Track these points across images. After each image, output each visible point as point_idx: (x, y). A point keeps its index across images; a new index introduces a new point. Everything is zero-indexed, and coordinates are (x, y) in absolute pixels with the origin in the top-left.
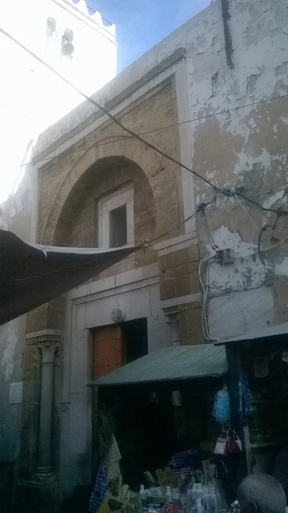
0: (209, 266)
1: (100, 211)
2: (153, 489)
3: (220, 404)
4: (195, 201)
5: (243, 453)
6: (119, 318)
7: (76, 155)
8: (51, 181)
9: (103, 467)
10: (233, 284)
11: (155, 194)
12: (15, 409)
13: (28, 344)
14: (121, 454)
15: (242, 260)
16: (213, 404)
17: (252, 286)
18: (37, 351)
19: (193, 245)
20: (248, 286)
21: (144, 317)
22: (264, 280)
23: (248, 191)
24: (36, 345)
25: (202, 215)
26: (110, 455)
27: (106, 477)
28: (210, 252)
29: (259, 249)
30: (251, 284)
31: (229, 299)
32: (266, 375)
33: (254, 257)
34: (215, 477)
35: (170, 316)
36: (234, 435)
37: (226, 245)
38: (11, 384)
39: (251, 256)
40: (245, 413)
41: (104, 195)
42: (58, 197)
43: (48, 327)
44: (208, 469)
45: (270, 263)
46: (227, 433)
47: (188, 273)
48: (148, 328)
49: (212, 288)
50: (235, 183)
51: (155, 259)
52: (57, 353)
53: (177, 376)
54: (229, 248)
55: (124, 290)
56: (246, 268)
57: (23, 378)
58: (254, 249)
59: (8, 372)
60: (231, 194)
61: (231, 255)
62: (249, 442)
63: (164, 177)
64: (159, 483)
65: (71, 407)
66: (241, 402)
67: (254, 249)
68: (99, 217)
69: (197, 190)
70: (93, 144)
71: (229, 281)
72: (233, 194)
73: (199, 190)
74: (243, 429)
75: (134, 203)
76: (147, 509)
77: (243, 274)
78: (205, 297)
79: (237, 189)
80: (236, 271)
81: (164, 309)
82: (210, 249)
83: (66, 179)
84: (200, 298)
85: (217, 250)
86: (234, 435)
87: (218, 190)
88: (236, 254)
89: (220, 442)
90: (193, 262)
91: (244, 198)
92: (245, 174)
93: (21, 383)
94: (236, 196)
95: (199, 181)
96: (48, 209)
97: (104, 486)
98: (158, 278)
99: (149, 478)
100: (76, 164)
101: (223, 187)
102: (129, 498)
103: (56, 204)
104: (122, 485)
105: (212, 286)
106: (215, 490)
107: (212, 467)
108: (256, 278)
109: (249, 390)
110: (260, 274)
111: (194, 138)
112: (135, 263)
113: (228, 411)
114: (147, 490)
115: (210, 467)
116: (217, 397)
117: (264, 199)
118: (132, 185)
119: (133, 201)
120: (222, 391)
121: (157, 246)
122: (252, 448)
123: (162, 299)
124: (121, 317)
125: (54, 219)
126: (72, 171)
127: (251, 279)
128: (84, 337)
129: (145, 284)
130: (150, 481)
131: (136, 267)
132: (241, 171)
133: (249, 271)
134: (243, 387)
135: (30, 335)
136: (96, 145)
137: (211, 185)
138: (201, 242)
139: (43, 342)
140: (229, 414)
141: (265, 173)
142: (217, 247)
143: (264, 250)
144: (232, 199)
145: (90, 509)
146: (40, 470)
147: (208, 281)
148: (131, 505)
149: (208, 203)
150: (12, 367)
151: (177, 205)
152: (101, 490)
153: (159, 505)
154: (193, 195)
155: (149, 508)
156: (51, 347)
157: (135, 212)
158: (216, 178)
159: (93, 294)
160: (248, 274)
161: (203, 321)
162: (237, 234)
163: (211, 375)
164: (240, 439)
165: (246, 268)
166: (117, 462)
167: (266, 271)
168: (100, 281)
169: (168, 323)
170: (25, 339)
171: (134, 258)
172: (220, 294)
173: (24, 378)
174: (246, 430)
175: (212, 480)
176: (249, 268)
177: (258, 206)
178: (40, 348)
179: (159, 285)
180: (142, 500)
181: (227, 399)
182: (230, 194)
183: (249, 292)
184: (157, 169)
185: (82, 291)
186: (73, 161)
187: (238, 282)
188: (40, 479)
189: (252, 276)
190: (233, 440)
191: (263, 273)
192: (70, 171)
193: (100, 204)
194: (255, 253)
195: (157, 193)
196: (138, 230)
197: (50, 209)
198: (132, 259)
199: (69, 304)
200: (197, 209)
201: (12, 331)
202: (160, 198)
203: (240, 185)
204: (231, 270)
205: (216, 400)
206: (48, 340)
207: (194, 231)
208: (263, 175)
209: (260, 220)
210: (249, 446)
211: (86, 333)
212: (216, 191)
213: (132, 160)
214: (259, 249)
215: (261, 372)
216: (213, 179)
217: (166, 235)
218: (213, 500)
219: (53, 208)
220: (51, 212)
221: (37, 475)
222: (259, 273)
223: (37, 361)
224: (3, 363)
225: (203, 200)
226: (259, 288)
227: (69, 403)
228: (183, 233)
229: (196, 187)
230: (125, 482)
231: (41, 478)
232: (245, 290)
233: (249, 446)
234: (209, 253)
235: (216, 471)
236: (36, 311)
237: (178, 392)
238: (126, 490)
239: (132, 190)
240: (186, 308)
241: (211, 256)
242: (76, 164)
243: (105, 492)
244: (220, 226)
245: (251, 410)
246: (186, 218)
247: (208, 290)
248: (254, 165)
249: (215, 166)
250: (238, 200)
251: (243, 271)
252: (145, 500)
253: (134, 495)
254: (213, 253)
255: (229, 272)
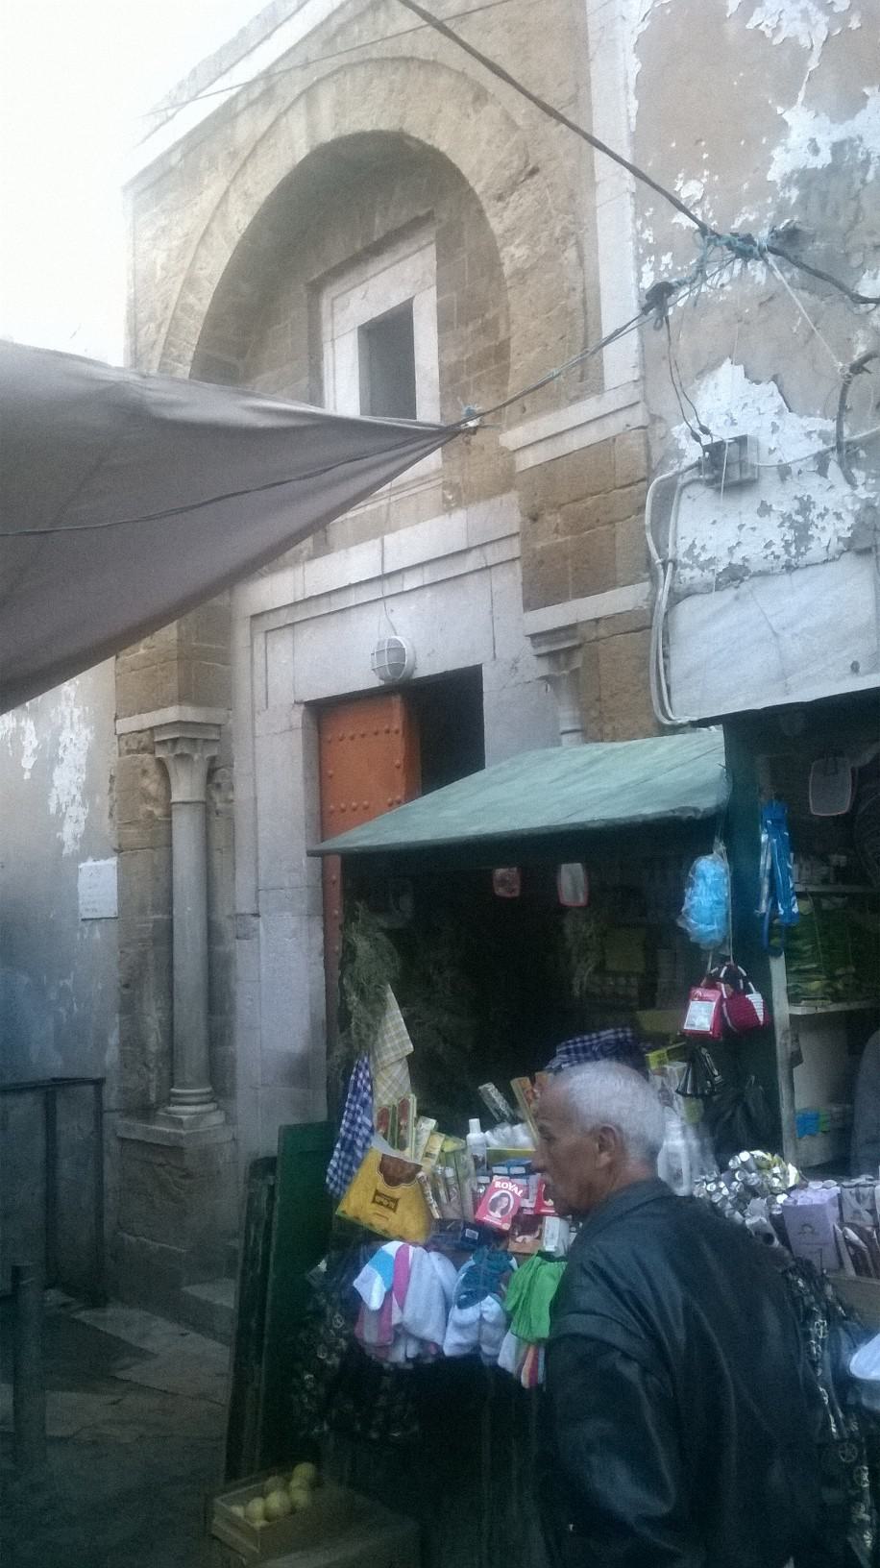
0: (680, 496)
1: (326, 328)
2: (506, 1130)
3: (704, 892)
4: (639, 279)
5: (765, 1032)
6: (397, 667)
7: (245, 130)
8: (163, 229)
9: (361, 1075)
10: (752, 551)
11: (507, 261)
12: (98, 935)
13: (126, 748)
14: (413, 1040)
15: (784, 472)
16: (683, 895)
17: (811, 556)
18: (152, 768)
19: (629, 428)
20: (799, 554)
21: (471, 664)
22: (849, 535)
23: (812, 238)
24: (151, 753)
25: (659, 322)
26: (380, 1040)
27: (370, 1101)
28: (684, 450)
29: (840, 432)
30: (807, 549)
31: (737, 598)
32: (844, 809)
33: (821, 462)
34: (684, 1095)
35: (552, 656)
36: (741, 981)
37: (736, 424)
38: (82, 865)
39: (811, 458)
40: (776, 921)
41: (338, 272)
42: (190, 283)
43: (183, 698)
44: (662, 1072)
45: (872, 478)
46: (722, 975)
47: (611, 523)
48: (485, 697)
49: (685, 566)
50: (770, 214)
51: (506, 480)
52: (215, 775)
53: (577, 819)
54: (744, 434)
55: (411, 582)
56: (796, 498)
57: (117, 847)
58: (823, 436)
59: (70, 833)
60: (756, 250)
61: (751, 457)
62: (786, 1000)
63: (536, 200)
64: (520, 1115)
65: (261, 925)
66: (766, 889)
67: (823, 436)
68: (325, 345)
69: (647, 240)
70: (297, 91)
71: (739, 543)
72: (762, 251)
73: (651, 241)
74: (768, 963)
75: (439, 294)
76: (489, 1181)
77: (786, 518)
78: (663, 595)
79: (775, 234)
80: (765, 509)
81: (533, 637)
82: (683, 438)
83: (212, 220)
84: (647, 600)
85: (706, 440)
86: (741, 981)
87: (713, 237)
88: (764, 452)
89: (701, 999)
90: (629, 485)
91: (802, 266)
92: (805, 178)
93: (113, 861)
94: (771, 258)
95: (651, 209)
96: (160, 326)
97: (366, 1126)
98: (516, 542)
99: (494, 1101)
100: (244, 165)
101: (732, 227)
102: (436, 1152)
103: (185, 308)
104: (417, 1120)
105: (685, 560)
106: (684, 1130)
107: (676, 1068)
108: (823, 529)
109: (792, 855)
110: (838, 516)
111: (637, 57)
112: (443, 495)
113: (727, 914)
114: (488, 1133)
115: (668, 1067)
116: (693, 873)
117: (862, 268)
118: (427, 236)
119: (434, 290)
120: (710, 857)
121: (513, 437)
122: (793, 1017)
123: (529, 605)
124: (404, 665)
125: (179, 356)
126: (232, 189)
127: (810, 533)
128: (291, 729)
129: (471, 562)
130: (498, 1111)
131: (447, 508)
132: (793, 172)
133: (805, 506)
134: (772, 845)
135: (129, 724)
136: (309, 94)
137: (694, 218)
138: (655, 419)
139: (169, 744)
140: (727, 921)
141: (870, 176)
142: (705, 431)
143: (855, 437)
144: (758, 271)
145: (327, 1180)
146: (178, 1095)
147: (675, 544)
148: (443, 1172)
149: (681, 284)
150: (83, 818)
151: (577, 297)
152: (358, 1135)
153: (522, 1170)
154: (630, 261)
155: (495, 1177)
156: (196, 757)
157: (444, 324)
158: (708, 198)
159: (311, 598)
160: (800, 519)
161: (653, 670)
162: (773, 386)
163: (677, 814)
164: (759, 990)
165: (796, 498)
166: (400, 1060)
167: (858, 507)
168: (334, 555)
169: (546, 678)
170: (115, 734)
171: (440, 481)
172: (708, 585)
173: (120, 846)
174: (778, 967)
175: (675, 1104)
176: (805, 499)
177: (841, 287)
178: (160, 762)
179: (518, 565)
180: (475, 1158)
181: (726, 880)
182: (751, 251)
183: (798, 577)
184: (513, 171)
185: (275, 589)
186: (233, 155)
187: (768, 545)
188: (180, 1119)
189: (813, 522)
190: (738, 996)
191: (848, 510)
192: (227, 192)
193: (325, 302)
194: (825, 447)
195: (514, 254)
196: (451, 381)
197: (168, 322)
198: (434, 484)
199: (242, 633)
200: (645, 302)
201: (72, 712)
202: (521, 275)
203: (787, 221)
204: (748, 503)
205: (692, 884)
206: (184, 738)
207: (635, 381)
208: (863, 181)
209: (849, 339)
210: (784, 1010)
211: (298, 716)
212: (707, 237)
213: (429, 142)
214: (840, 432)
215: (831, 800)
216: (699, 203)
217: (542, 393)
218: (676, 1155)
219: (173, 318)
220: (169, 333)
221: (172, 1108)
222: (835, 513)
223: (156, 800)
224: (53, 810)
225: (666, 275)
226: (834, 559)
227: (257, 915)
228: (598, 388)
229: (643, 231)
230: (422, 1113)
231: (185, 1118)
232: (789, 568)
233: (784, 1010)
234: (680, 454)
235: (686, 1080)
236: (142, 651)
237: (578, 867)
238: (428, 1133)
239: (431, 251)
240: (602, 632)
241: (687, 462)
242: (244, 165)
243: (367, 1139)
244: (717, 364)
245: (795, 910)
246: (606, 332)
247: (673, 574)
248: (837, 148)
249: (705, 156)
250: (778, 274)
251: (786, 509)
252: (483, 1160)
253: (451, 1145)
254: (694, 452)
255: (740, 513)
